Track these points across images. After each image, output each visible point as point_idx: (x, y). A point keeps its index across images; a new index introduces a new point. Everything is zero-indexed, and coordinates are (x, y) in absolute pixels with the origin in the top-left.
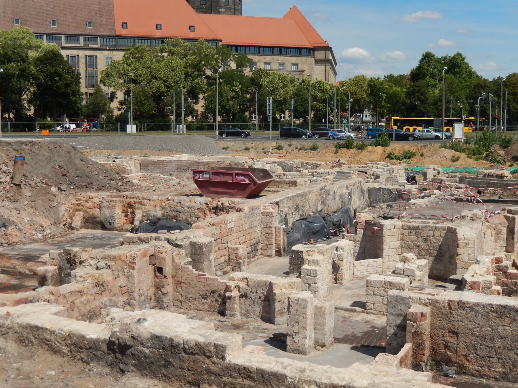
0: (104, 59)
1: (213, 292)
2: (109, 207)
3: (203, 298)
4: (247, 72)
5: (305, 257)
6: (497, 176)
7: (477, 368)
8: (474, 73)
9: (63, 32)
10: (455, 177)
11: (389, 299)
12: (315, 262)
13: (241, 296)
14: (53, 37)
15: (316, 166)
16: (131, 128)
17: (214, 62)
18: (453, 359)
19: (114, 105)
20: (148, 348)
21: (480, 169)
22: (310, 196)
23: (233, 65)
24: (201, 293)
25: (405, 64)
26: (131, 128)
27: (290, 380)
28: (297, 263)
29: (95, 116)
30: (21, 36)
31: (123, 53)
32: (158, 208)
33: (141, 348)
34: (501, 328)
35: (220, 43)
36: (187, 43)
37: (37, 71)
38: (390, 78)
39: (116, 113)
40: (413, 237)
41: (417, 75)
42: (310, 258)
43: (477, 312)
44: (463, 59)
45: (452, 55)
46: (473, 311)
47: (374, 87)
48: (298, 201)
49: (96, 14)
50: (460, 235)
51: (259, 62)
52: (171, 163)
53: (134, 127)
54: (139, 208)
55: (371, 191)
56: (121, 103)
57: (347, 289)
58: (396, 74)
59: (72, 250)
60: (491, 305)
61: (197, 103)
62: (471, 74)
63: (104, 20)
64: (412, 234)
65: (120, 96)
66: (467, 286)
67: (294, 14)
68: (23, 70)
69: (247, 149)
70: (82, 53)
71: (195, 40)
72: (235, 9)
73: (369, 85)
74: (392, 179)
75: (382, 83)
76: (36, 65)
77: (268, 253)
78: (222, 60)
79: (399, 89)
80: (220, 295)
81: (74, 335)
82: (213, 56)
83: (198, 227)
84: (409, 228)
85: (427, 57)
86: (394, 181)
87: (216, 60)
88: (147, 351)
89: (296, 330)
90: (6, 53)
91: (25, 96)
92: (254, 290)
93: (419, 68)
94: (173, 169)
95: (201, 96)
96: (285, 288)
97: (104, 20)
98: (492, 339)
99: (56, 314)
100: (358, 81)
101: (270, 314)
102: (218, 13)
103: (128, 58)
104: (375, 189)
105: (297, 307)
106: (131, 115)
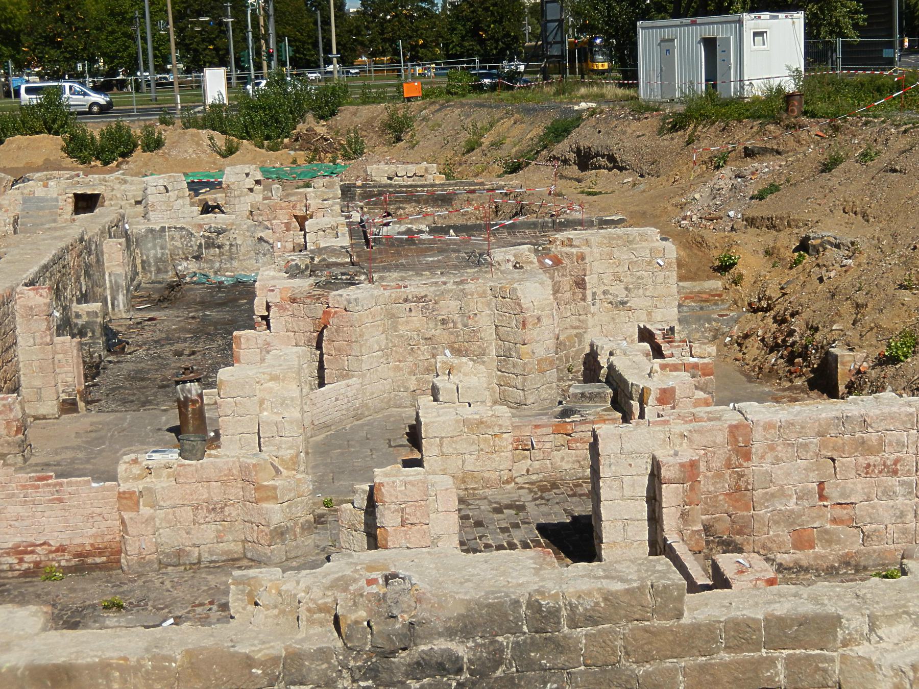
40: (417, 319)
64: (413, 314)
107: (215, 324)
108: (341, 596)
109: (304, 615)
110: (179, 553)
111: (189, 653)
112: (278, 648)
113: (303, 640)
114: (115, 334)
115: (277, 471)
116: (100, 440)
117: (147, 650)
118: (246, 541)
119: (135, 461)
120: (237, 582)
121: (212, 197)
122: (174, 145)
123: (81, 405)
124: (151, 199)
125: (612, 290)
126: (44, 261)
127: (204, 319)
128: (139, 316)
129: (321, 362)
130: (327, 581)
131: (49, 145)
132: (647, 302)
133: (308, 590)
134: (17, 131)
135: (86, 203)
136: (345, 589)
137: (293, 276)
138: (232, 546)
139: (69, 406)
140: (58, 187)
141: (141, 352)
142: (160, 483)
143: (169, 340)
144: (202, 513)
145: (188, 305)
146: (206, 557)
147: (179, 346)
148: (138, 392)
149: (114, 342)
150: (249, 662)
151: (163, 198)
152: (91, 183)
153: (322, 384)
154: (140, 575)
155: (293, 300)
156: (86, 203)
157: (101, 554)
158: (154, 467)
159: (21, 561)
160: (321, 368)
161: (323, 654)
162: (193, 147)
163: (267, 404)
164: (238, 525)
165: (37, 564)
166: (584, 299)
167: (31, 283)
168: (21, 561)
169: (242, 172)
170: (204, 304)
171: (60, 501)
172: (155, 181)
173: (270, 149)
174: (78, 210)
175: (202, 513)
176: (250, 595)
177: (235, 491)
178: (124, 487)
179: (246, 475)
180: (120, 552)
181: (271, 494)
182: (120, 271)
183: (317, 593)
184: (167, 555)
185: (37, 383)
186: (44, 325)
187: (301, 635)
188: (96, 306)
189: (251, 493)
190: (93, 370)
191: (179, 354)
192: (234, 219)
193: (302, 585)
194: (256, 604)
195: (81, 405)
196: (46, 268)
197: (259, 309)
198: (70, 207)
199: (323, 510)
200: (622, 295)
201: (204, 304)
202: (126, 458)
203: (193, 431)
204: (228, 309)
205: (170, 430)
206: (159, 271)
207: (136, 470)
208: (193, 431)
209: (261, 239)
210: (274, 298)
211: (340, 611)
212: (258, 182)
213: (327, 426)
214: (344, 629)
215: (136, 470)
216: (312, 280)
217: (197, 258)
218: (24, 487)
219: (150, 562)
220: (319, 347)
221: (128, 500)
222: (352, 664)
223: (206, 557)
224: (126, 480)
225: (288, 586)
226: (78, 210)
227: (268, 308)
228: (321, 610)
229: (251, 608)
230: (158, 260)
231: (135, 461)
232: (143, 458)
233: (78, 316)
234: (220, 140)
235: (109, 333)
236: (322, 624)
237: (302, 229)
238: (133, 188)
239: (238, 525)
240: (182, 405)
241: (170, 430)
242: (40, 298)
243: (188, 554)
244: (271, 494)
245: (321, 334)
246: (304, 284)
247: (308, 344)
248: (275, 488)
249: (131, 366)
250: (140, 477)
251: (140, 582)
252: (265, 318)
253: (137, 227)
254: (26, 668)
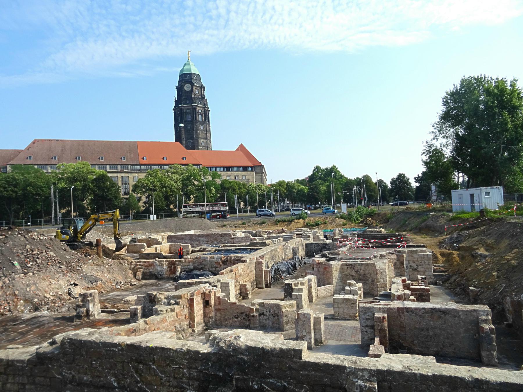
0: (134, 178)
1: (242, 313)
2: (159, 265)
3: (236, 318)
4: (218, 181)
5: (294, 287)
6: (378, 232)
7: (420, 349)
8: (343, 176)
9: (107, 163)
10: (355, 234)
11: (361, 309)
12: (301, 290)
13: (260, 315)
14: (101, 166)
15: (270, 233)
16: (153, 217)
17: (199, 177)
18: (404, 345)
19: (141, 204)
20: (246, 355)
22: (278, 250)
23: (210, 178)
24: (234, 315)
25: (306, 173)
26: (153, 217)
27: (348, 370)
28: (289, 292)
29: (131, 212)
30: (82, 166)
31: (145, 174)
32: (191, 264)
33: (240, 356)
34: (432, 323)
35: (201, 166)
36: (182, 167)
37: (94, 186)
38: (298, 181)
39: (143, 208)
40: (349, 270)
41: (312, 178)
42: (297, 288)
43: (416, 314)
44: (337, 169)
45: (330, 167)
46: (413, 313)
47: (289, 186)
48: (273, 253)
49: (127, 152)
50: (378, 267)
51: (224, 175)
52: (186, 235)
53: (155, 216)
54: (178, 265)
55: (306, 244)
56: (145, 203)
57: (317, 305)
58: (300, 179)
59: (152, 294)
60: (424, 309)
61: (190, 200)
62: (342, 177)
63: (132, 155)
65: (144, 198)
66: (396, 298)
67: (242, 148)
68: (84, 186)
69: (224, 226)
70: (119, 175)
71: (187, 165)
72: (208, 146)
73: (287, 185)
74: (316, 238)
75: (294, 184)
76: (92, 183)
77: (261, 286)
78: (203, 175)
79: (304, 187)
80: (246, 315)
81: (191, 351)
82: (198, 173)
83: (222, 274)
84: (346, 265)
85: (317, 168)
86: (318, 238)
87: (200, 175)
88: (245, 358)
89: (304, 334)
90: (74, 177)
91: (85, 202)
92: (268, 310)
93: (313, 175)
94: (187, 239)
95: (192, 196)
96: (288, 307)
97: (132, 155)
98: (428, 330)
99: (170, 338)
100: (281, 184)
101: (279, 325)
102: (198, 149)
103: (148, 177)
104: (309, 244)
105: (304, 319)
106: (153, 209)
125: (413, 265)
132: (423, 270)
166: (403, 267)
200: (416, 267)
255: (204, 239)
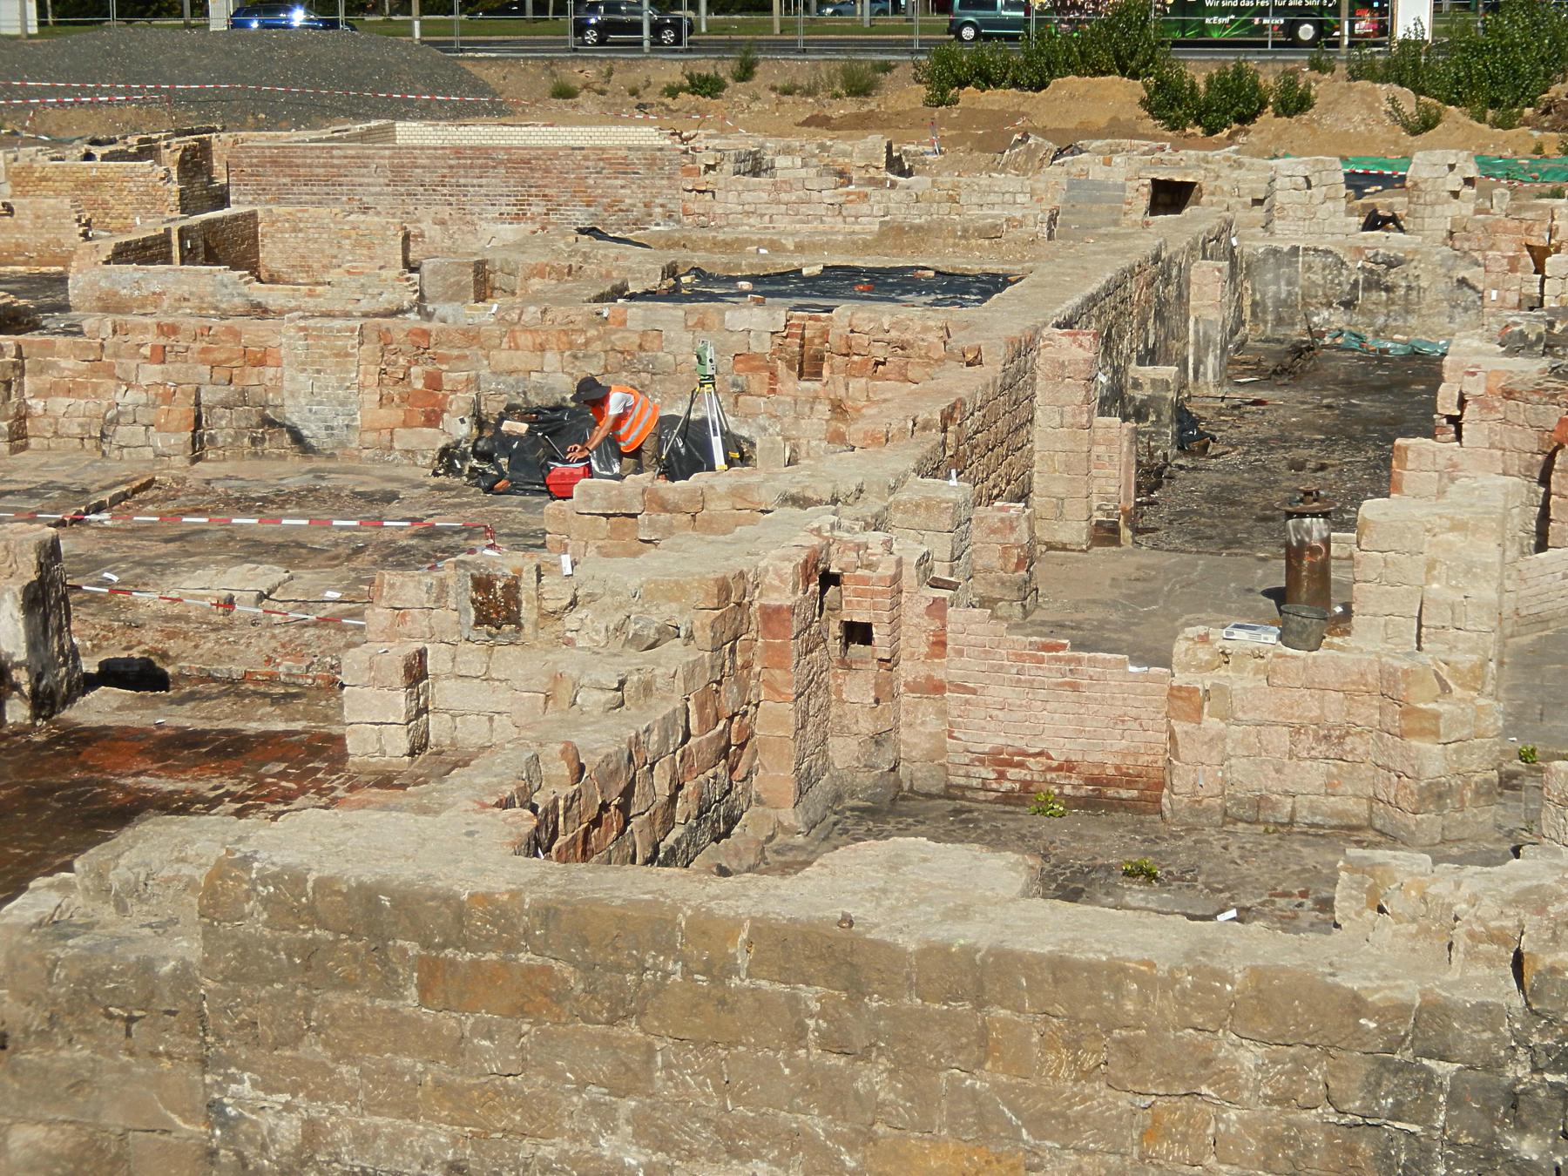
21: (654, 159)
107: (1366, 421)
108: (1531, 921)
109: (1461, 945)
110: (1260, 803)
111: (1256, 973)
112: (1410, 991)
113: (1454, 985)
114: (1195, 422)
115: (1445, 688)
116: (1149, 596)
117: (1188, 956)
118: (1375, 798)
119: (1204, 639)
120: (1353, 867)
121: (1385, 201)
122: (1331, 106)
123: (1126, 533)
124: (1280, 198)
126: (1092, 289)
127: (1348, 411)
128: (1237, 395)
129: (1545, 507)
130: (1510, 890)
131: (1121, 94)
133: (1474, 900)
134: (1070, 68)
135: (1170, 196)
136: (1541, 910)
137: (1513, 352)
138: (1350, 805)
139: (1105, 534)
140: (1128, 168)
141: (1234, 457)
142: (1241, 681)
143: (1283, 440)
144: (1307, 741)
145: (1323, 384)
146: (1304, 816)
147: (1300, 453)
148: (1223, 522)
149: (1191, 434)
150: (1356, 1005)
151: (1303, 195)
152: (1183, 161)
153: (1541, 546)
154: (1190, 829)
155: (1508, 394)
156: (1170, 196)
157: (1130, 784)
158: (1235, 652)
159: (1001, 776)
160: (1544, 518)
161: (1487, 1014)
162: (1358, 111)
163: (1440, 570)
164: (1365, 770)
165: (1026, 785)
167: (1068, 324)
168: (1001, 776)
169: (1442, 163)
170: (1351, 386)
171: (1075, 687)
172: (1291, 168)
173: (1495, 124)
174: (1156, 207)
175: (1307, 741)
176: (1373, 892)
177: (1368, 712)
178: (1180, 679)
179: (1390, 687)
180: (1161, 785)
181: (1428, 726)
182: (1214, 315)
183: (1489, 908)
184: (1240, 803)
185: (1059, 489)
186: (1080, 396)
187: (1453, 975)
188: (1168, 372)
189: (1394, 720)
190: (1151, 477)
191: (1298, 466)
192: (1420, 242)
193: (1465, 891)
194: (1381, 910)
195: (1126, 533)
196: (1093, 300)
197: (1446, 404)
198: (1144, 202)
199: (1517, 765)
201: (1351, 386)
202: (1190, 632)
203: (1307, 599)
204: (1393, 399)
205: (1268, 593)
206: (1279, 321)
207: (1204, 654)
208: (1307, 599)
209: (1463, 282)
210: (1474, 388)
211: (1526, 947)
212: (1469, 182)
213: (1541, 621)
214: (1529, 977)
215: (1204, 654)
216: (1545, 362)
217: (1348, 305)
218: (1020, 657)
219: (1208, 810)
220: (1545, 480)
221: (1186, 702)
222: (1535, 1039)
223: (1304, 816)
224: (1186, 667)
225: (1440, 888)
226: (1156, 207)
227: (1462, 403)
228: (1492, 938)
229: (1371, 914)
230: (1280, 303)
231: (1204, 639)
232: (1217, 634)
233: (1137, 385)
234: (1408, 101)
235: (1183, 418)
236: (1490, 962)
237: (1539, 270)
238: (1252, 177)
239: (1365, 770)
240: (1294, 554)
241: (1268, 593)
242: (1078, 349)
243: (1274, 806)
244: (1428, 726)
245: (1551, 458)
246: (1531, 367)
247: (1526, 473)
248: (1437, 716)
249: (1215, 479)
250: (1208, 667)
251: (1189, 841)
252: (1455, 421)
253: (1251, 244)
254: (989, 952)
255: (495, 182)
